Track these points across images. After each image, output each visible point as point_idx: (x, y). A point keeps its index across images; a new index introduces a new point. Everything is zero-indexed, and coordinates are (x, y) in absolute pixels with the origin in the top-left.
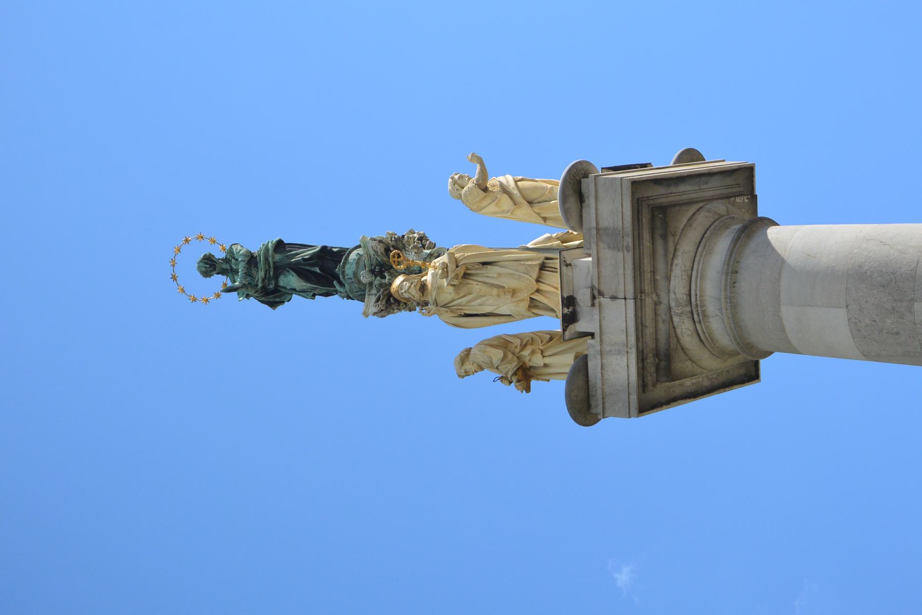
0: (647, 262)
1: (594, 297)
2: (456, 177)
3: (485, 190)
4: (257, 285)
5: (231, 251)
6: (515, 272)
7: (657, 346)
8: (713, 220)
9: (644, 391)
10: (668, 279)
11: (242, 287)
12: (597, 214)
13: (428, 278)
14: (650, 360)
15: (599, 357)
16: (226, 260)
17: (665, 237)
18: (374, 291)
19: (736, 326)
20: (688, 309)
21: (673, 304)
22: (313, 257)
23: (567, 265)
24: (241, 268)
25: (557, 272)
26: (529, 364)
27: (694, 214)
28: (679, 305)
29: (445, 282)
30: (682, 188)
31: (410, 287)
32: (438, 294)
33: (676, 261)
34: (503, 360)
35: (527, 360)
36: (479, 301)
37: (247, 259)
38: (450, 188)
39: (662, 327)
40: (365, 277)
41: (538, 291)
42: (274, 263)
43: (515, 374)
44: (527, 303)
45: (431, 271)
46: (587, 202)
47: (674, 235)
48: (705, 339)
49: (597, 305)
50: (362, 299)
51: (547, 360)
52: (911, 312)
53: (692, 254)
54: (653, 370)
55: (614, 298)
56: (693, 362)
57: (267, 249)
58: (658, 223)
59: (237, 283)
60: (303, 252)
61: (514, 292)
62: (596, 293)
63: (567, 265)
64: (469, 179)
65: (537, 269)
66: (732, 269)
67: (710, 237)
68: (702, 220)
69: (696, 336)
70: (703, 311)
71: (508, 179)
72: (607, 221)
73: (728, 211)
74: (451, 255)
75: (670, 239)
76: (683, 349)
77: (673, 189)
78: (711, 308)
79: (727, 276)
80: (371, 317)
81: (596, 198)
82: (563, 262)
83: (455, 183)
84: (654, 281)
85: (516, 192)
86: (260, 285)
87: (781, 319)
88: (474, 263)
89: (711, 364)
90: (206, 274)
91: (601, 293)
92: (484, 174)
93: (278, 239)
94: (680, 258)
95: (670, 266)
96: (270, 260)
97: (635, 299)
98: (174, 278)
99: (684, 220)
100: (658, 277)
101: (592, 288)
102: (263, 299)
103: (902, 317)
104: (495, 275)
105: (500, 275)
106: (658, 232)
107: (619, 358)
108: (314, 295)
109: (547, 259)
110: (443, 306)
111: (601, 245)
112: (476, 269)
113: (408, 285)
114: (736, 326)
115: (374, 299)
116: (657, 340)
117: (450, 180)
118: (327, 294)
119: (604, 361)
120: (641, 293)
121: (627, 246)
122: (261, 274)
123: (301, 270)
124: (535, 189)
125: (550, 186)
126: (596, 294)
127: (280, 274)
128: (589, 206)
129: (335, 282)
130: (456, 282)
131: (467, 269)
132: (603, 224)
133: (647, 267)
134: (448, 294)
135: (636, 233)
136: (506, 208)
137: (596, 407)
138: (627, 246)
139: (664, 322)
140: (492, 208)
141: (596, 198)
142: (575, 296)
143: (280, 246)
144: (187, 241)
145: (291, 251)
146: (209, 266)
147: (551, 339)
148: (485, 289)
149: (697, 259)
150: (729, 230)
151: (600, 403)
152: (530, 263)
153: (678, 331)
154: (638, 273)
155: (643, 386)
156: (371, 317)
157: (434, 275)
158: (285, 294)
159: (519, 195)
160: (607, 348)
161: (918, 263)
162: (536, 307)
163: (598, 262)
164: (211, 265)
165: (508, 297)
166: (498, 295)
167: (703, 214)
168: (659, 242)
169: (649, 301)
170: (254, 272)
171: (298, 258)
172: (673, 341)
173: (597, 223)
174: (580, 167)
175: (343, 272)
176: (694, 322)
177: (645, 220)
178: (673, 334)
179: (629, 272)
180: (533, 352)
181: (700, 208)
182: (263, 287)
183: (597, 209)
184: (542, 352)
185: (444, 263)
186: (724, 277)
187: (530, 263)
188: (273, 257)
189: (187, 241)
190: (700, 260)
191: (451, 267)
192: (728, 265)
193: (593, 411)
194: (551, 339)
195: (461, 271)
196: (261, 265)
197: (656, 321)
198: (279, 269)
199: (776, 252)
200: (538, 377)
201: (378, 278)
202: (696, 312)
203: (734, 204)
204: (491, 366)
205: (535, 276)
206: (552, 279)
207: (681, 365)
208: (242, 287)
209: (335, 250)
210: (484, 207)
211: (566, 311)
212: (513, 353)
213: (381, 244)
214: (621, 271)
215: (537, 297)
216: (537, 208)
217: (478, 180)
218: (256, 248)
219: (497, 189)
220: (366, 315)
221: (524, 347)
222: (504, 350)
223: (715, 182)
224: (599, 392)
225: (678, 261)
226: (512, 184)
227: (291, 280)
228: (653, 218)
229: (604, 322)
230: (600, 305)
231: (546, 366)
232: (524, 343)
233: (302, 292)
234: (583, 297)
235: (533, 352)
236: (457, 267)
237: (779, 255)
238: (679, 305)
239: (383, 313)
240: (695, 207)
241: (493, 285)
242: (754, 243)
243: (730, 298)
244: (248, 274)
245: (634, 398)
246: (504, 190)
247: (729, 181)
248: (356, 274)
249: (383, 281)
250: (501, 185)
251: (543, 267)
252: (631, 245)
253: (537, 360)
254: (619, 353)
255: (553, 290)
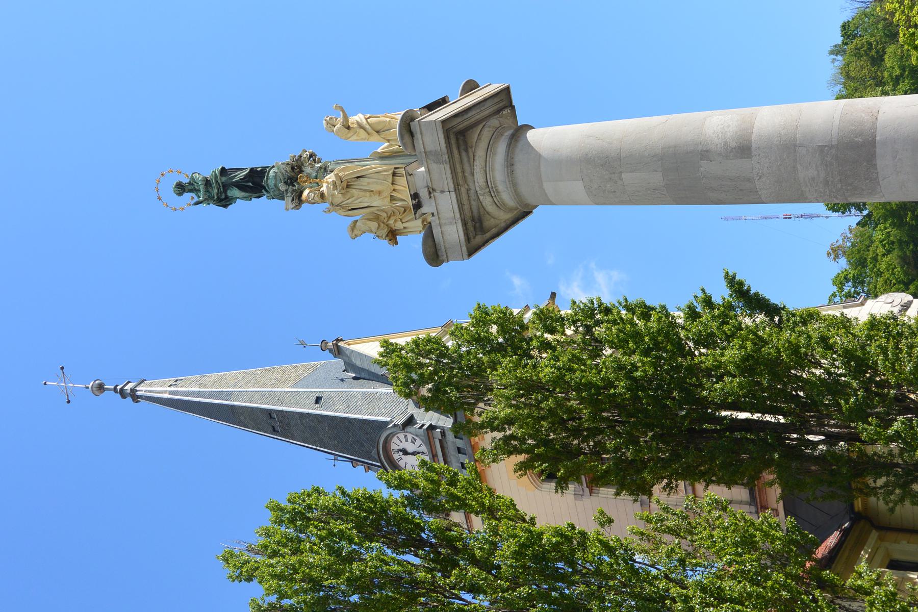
0: (458, 166)
1: (430, 193)
2: (328, 119)
3: (348, 128)
4: (214, 197)
5: (192, 178)
6: (378, 180)
7: (472, 215)
8: (493, 132)
9: (469, 242)
10: (473, 174)
11: (205, 200)
12: (423, 143)
13: (324, 189)
14: (470, 224)
15: (439, 227)
16: (190, 184)
17: (466, 151)
18: (289, 194)
19: (517, 195)
20: (488, 190)
21: (478, 189)
22: (246, 176)
23: (410, 175)
24: (202, 188)
25: (403, 176)
26: (394, 228)
27: (481, 131)
28: (481, 189)
29: (336, 192)
30: (470, 114)
31: (314, 196)
32: (332, 199)
33: (475, 163)
34: (378, 228)
35: (393, 226)
36: (359, 200)
37: (204, 183)
38: (325, 126)
39: (474, 203)
40: (282, 187)
41: (394, 190)
42: (222, 183)
43: (387, 235)
44: (389, 199)
45: (325, 185)
46: (416, 136)
47: (472, 147)
48: (500, 205)
49: (433, 197)
50: (282, 198)
51: (405, 225)
52: (621, 179)
53: (485, 157)
54: (472, 229)
55: (442, 192)
56: (495, 218)
57: (216, 175)
58: (461, 143)
59: (201, 198)
60: (239, 174)
61: (380, 193)
62: (431, 190)
63: (410, 175)
64: (336, 119)
65: (391, 176)
66: (510, 164)
67: (493, 144)
68: (486, 134)
69: (494, 204)
70: (496, 190)
71: (359, 118)
72: (430, 147)
73: (500, 123)
74: (336, 175)
75: (470, 150)
76: (488, 213)
77: (466, 117)
78: (501, 187)
79: (508, 168)
80: (290, 210)
81: (421, 134)
82: (407, 174)
83: (328, 123)
84: (464, 177)
85: (368, 126)
86: (216, 198)
87: (544, 190)
88: (352, 178)
89: (505, 216)
90: (180, 194)
91: (434, 190)
92: (346, 118)
93: (221, 167)
94: (478, 161)
95: (472, 167)
96: (219, 181)
97: (455, 191)
98: (159, 198)
99: (476, 136)
100: (467, 175)
101: (428, 187)
102: (219, 204)
103: (616, 182)
104: (366, 184)
105: (369, 183)
106: (462, 147)
107: (451, 226)
108: (251, 199)
109: (396, 168)
110: (337, 206)
111: (429, 162)
112: (355, 181)
113: (313, 195)
114: (517, 195)
115: (290, 199)
116: (472, 211)
117: (324, 122)
118: (259, 197)
119: (443, 229)
120: (458, 185)
121: (445, 161)
122: (215, 191)
123: (240, 186)
124: (380, 122)
125: (388, 119)
126: (431, 191)
127: (228, 189)
128: (418, 139)
129: (263, 191)
130: (343, 192)
131: (348, 182)
132: (428, 149)
133: (459, 170)
134: (339, 198)
135: (449, 151)
136: (364, 137)
137: (443, 256)
138: (445, 161)
139: (474, 200)
140: (355, 137)
141: (421, 134)
142: (418, 192)
143: (223, 171)
144: (162, 174)
145: (231, 174)
146: (181, 188)
147: (405, 211)
148: (361, 193)
149: (488, 159)
150: (504, 137)
151: (444, 253)
152: (385, 173)
153: (484, 204)
154: (454, 174)
155: (468, 239)
156: (290, 210)
157: (327, 187)
158: (232, 199)
159: (370, 128)
160: (443, 221)
161: (621, 149)
162: (395, 200)
163: (429, 171)
164: (182, 189)
165: (377, 196)
166: (370, 196)
167: (486, 130)
168: (464, 154)
169: (463, 190)
170: (210, 189)
171: (237, 179)
172: (482, 210)
173: (424, 149)
174: (407, 115)
175: (268, 185)
176: (492, 197)
177: (453, 141)
178: (481, 206)
179: (449, 175)
180: (396, 221)
181: (484, 126)
182: (218, 198)
183: (423, 140)
184: (401, 220)
185: (333, 181)
186: (506, 169)
187: (385, 173)
188: (221, 179)
189: (162, 174)
190: (489, 160)
191: (338, 182)
192: (507, 162)
193: (441, 259)
194: (405, 211)
195: (345, 184)
196: (214, 185)
197: (469, 200)
198: (226, 187)
199: (535, 150)
200: (400, 234)
201: (291, 187)
202: (491, 190)
203: (501, 117)
204: (371, 231)
205: (391, 181)
206: (402, 181)
207: (488, 222)
208: (205, 200)
209: (259, 169)
210: (350, 137)
211: (414, 202)
212: (383, 223)
213: (289, 166)
214: (444, 176)
215: (394, 194)
216: (383, 135)
217: (343, 122)
218: (208, 174)
219: (355, 126)
220: (287, 209)
221: (389, 218)
222: (463, 511)
223: (489, 103)
224: (443, 247)
225: (477, 163)
226: (364, 121)
227: (234, 192)
228: (457, 139)
229: (438, 206)
230: (434, 197)
231: (405, 228)
232: (389, 215)
233: (244, 198)
234: (423, 194)
235: (396, 221)
236: (342, 182)
237: (537, 151)
238: (481, 189)
239: (298, 207)
240: (481, 126)
241: (366, 191)
242: (520, 144)
243: (512, 181)
244: (207, 191)
245: (464, 249)
246: (360, 126)
247: (496, 100)
248: (275, 185)
249: (294, 188)
250: (358, 122)
251: (394, 174)
252: (447, 160)
253: (399, 226)
254: (451, 223)
255: (404, 188)
